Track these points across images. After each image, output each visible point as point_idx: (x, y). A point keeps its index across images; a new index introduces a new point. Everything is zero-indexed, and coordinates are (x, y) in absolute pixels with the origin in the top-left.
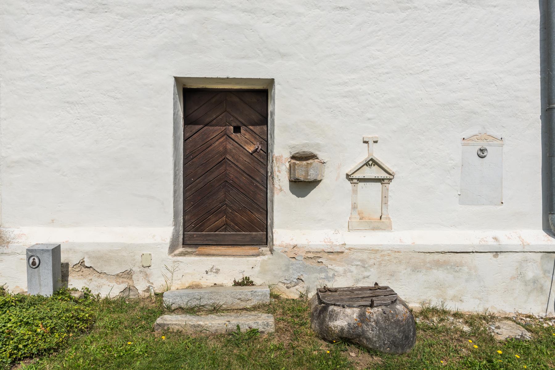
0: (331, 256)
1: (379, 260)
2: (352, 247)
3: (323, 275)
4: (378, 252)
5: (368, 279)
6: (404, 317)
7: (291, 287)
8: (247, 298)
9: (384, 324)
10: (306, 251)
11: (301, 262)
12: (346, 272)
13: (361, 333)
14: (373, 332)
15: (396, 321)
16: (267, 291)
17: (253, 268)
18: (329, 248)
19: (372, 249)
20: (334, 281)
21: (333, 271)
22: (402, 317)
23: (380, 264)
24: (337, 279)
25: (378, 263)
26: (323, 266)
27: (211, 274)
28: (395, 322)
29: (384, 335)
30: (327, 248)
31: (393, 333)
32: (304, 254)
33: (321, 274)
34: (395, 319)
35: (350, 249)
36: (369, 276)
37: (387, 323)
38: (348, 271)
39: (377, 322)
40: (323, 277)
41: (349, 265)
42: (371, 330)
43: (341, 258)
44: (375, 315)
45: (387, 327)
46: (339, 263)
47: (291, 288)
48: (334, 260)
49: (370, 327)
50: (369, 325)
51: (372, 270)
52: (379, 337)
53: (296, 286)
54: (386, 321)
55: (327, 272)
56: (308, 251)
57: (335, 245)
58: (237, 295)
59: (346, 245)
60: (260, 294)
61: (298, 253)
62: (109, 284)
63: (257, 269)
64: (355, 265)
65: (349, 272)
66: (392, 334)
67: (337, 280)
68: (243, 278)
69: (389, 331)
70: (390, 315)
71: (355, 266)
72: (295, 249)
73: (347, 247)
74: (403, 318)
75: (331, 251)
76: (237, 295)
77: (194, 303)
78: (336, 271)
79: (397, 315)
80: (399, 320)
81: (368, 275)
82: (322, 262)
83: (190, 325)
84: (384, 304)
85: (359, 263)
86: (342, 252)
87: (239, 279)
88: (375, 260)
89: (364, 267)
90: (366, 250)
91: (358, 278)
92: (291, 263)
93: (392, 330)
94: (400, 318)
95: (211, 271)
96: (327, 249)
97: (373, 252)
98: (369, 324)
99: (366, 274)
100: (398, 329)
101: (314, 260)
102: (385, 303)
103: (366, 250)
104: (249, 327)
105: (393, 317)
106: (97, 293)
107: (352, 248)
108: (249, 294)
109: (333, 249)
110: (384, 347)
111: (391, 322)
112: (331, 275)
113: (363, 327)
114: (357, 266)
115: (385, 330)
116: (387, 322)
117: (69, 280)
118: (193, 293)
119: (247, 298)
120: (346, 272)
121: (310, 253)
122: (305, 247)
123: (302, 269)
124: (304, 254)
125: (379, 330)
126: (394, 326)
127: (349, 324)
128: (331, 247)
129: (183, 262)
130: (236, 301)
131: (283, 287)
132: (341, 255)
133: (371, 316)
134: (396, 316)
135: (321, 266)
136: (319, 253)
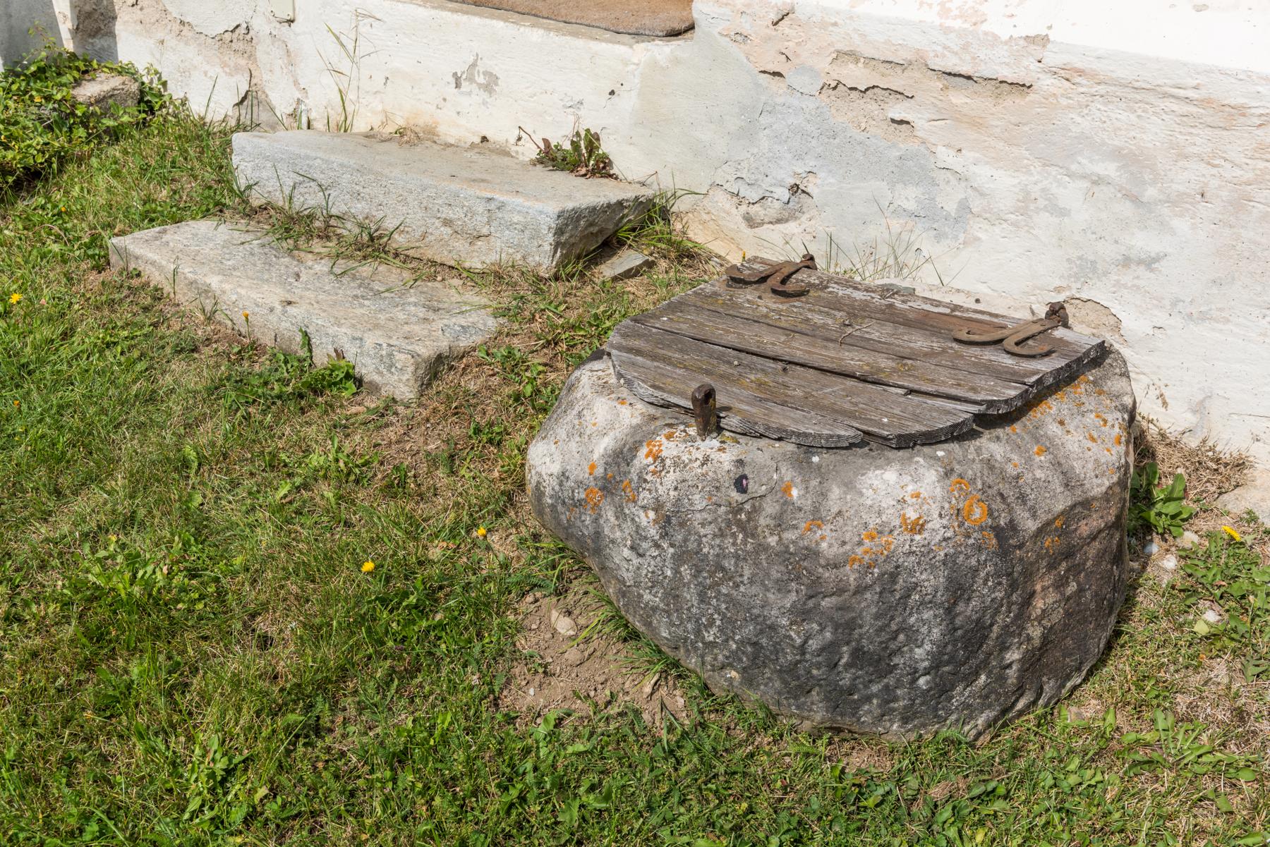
0: (960, 98)
1: (1238, 172)
2: (1079, 65)
3: (909, 197)
4: (1242, 119)
5: (1148, 274)
6: (860, 543)
7: (762, 224)
8: (471, 226)
9: (718, 541)
10: (840, 46)
11: (810, 104)
12: (1032, 206)
13: (589, 541)
14: (640, 560)
15: (792, 549)
16: (541, 212)
17: (612, 93)
18: (956, 49)
19: (1202, 94)
20: (961, 241)
21: (963, 184)
22: (844, 543)
23: (1240, 203)
24: (980, 235)
25: (1224, 194)
26: (913, 146)
27: (470, 93)
28: (787, 552)
29: (703, 598)
30: (939, 49)
31: (763, 607)
32: (823, 64)
33: (899, 186)
34: (790, 535)
35: (1068, 74)
36: (1156, 259)
37: (734, 544)
38: (1042, 203)
39: (670, 519)
40: (911, 206)
41: (1053, 170)
42: (632, 548)
43: (1013, 119)
44: (671, 477)
45: (729, 564)
46: (1001, 145)
47: (766, 226)
48: (976, 123)
49: (628, 527)
50: (625, 515)
51: (1181, 225)
52: (673, 595)
53: (787, 221)
54: (735, 529)
55: (934, 183)
56: (846, 49)
57: (986, 34)
58: (440, 202)
59: (1049, 46)
60: (516, 218)
61: (798, 56)
62: (207, 67)
63: (628, 101)
64: (1084, 177)
65: (1045, 209)
66: (756, 611)
67: (979, 239)
68: (578, 134)
69: (737, 586)
70: (770, 508)
71: (1085, 184)
72: (787, 31)
73: (1053, 58)
74: (848, 547)
75: (964, 70)
76: (440, 202)
77: (308, 199)
78: (975, 189)
79: (817, 518)
80: (812, 553)
81: (1153, 255)
82: (908, 123)
83: (185, 278)
84: (799, 435)
85: (1109, 169)
86: (1025, 87)
87: (561, 138)
88: (1214, 171)
89: (1136, 200)
90: (1166, 95)
91: (1092, 258)
92: (763, 98)
93: (754, 590)
94: (824, 545)
95: (471, 79)
96: (944, 56)
97: (1209, 120)
98: (627, 511)
99: (1143, 242)
100: (793, 597)
101: (874, 106)
102: (806, 435)
103: (1166, 95)
104: (336, 351)
105: (780, 524)
106: (182, 95)
107: (1081, 72)
108: (481, 210)
109: (974, 58)
110: (702, 656)
111: (766, 548)
112: (951, 207)
113: (600, 515)
114: (1094, 183)
115: (712, 574)
116: (734, 535)
117: (117, 32)
118: (307, 157)
119: (471, 226)
120: (1032, 206)
121: (857, 61)
122: (835, 24)
123: (814, 142)
124: (823, 64)
125: (679, 559)
126: (775, 574)
127: (563, 476)
128: (965, 47)
129: (385, 22)
130: (437, 228)
131: (728, 213)
132: (1014, 102)
133: (649, 477)
134: (803, 525)
135: (903, 144)
136: (899, 69)
